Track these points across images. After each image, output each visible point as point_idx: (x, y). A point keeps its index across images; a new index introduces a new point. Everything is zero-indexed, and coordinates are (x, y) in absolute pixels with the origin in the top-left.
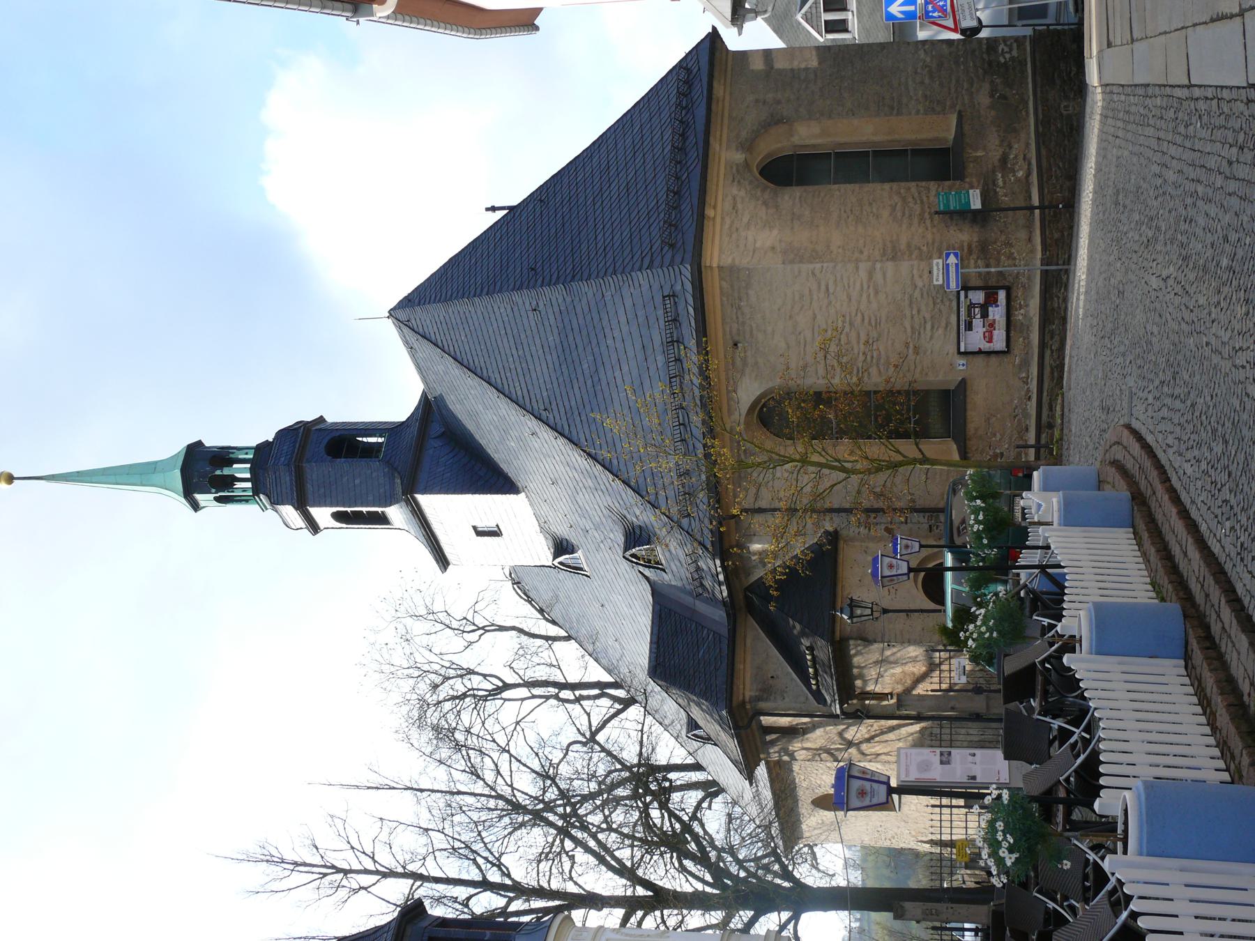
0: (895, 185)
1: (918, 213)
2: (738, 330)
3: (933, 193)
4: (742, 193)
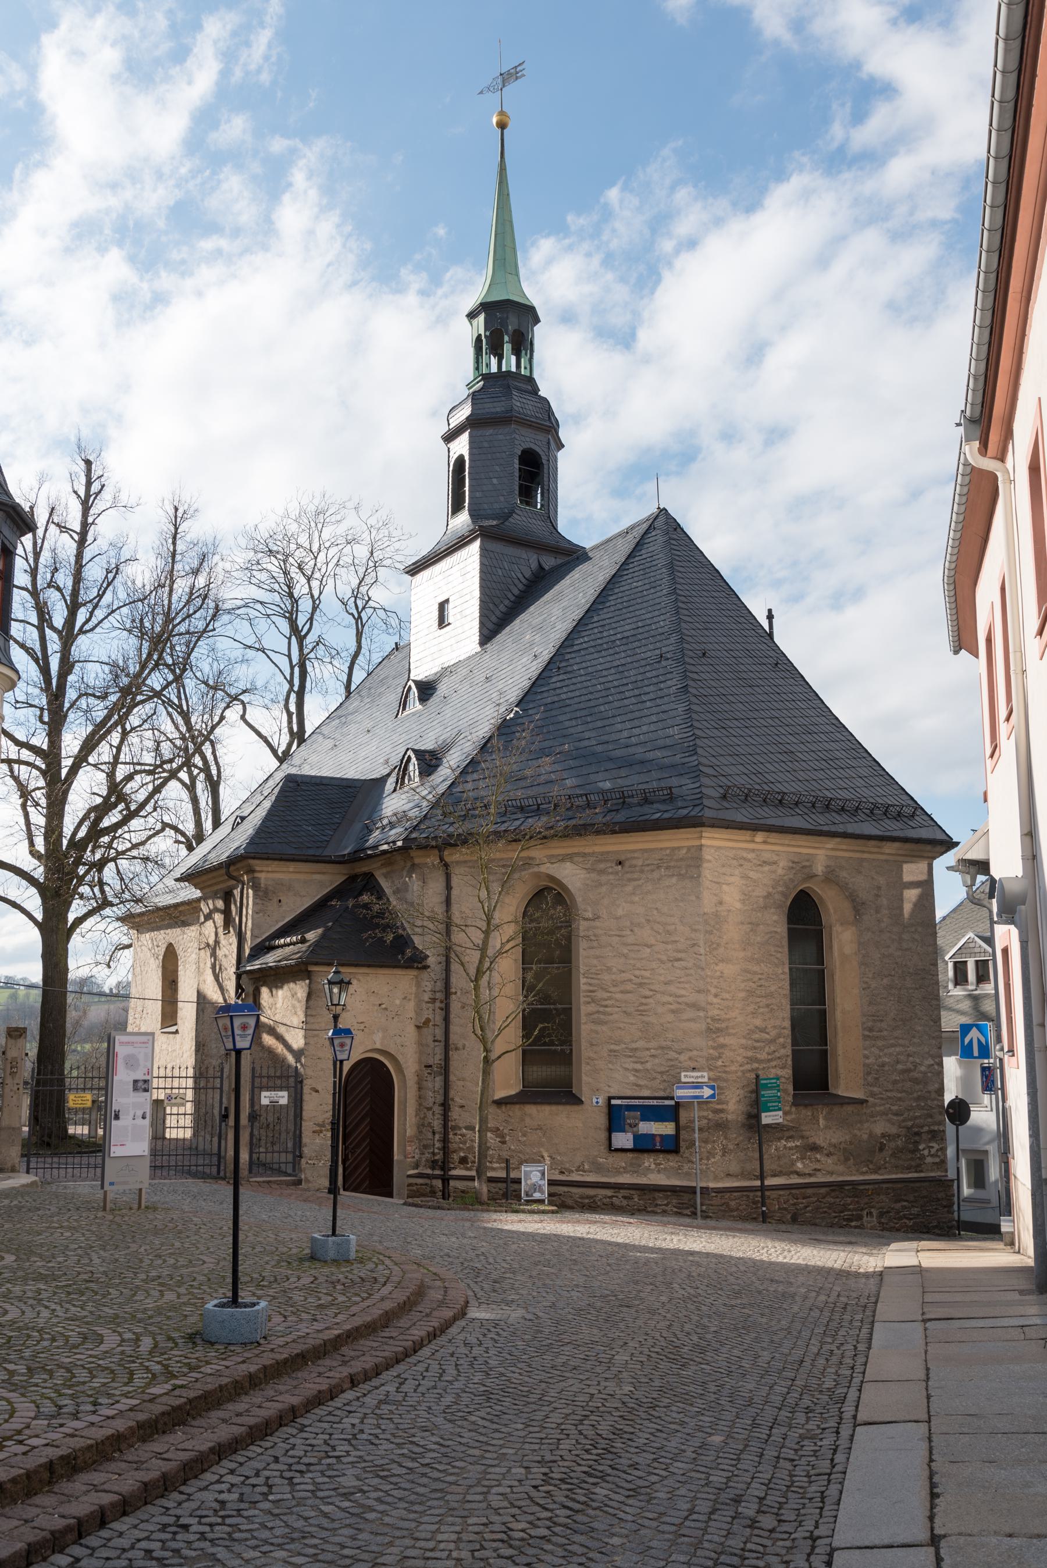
0: (788, 1032)
1: (758, 1056)
2: (635, 866)
3: (780, 1072)
4: (780, 871)
